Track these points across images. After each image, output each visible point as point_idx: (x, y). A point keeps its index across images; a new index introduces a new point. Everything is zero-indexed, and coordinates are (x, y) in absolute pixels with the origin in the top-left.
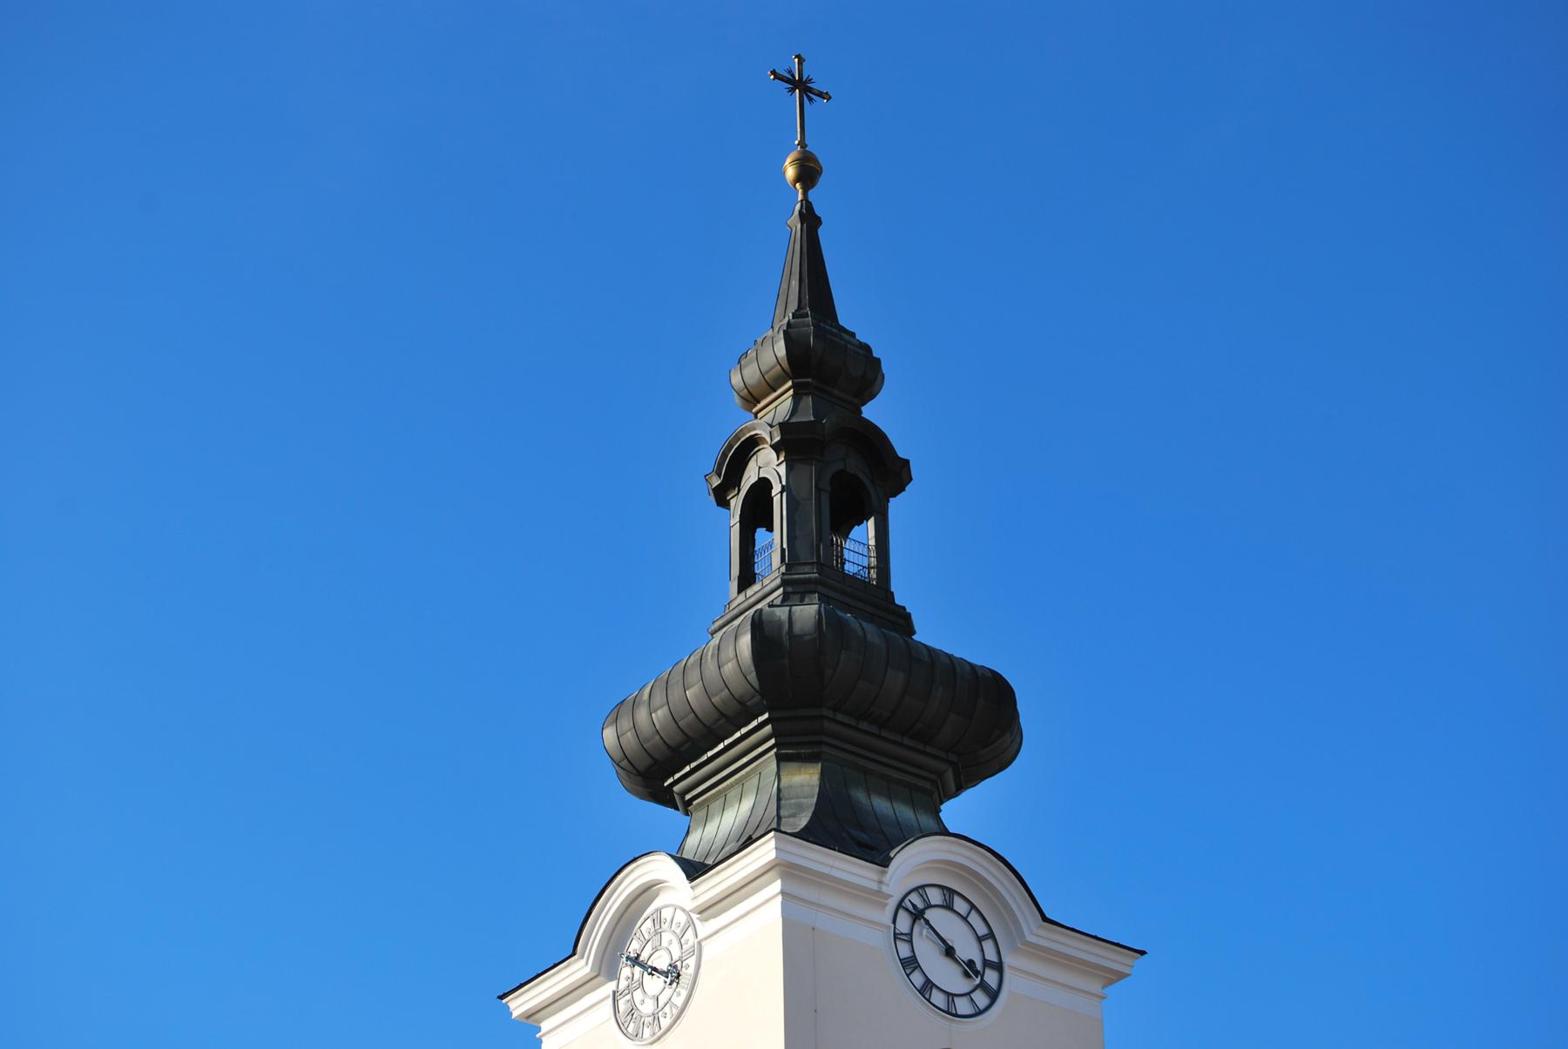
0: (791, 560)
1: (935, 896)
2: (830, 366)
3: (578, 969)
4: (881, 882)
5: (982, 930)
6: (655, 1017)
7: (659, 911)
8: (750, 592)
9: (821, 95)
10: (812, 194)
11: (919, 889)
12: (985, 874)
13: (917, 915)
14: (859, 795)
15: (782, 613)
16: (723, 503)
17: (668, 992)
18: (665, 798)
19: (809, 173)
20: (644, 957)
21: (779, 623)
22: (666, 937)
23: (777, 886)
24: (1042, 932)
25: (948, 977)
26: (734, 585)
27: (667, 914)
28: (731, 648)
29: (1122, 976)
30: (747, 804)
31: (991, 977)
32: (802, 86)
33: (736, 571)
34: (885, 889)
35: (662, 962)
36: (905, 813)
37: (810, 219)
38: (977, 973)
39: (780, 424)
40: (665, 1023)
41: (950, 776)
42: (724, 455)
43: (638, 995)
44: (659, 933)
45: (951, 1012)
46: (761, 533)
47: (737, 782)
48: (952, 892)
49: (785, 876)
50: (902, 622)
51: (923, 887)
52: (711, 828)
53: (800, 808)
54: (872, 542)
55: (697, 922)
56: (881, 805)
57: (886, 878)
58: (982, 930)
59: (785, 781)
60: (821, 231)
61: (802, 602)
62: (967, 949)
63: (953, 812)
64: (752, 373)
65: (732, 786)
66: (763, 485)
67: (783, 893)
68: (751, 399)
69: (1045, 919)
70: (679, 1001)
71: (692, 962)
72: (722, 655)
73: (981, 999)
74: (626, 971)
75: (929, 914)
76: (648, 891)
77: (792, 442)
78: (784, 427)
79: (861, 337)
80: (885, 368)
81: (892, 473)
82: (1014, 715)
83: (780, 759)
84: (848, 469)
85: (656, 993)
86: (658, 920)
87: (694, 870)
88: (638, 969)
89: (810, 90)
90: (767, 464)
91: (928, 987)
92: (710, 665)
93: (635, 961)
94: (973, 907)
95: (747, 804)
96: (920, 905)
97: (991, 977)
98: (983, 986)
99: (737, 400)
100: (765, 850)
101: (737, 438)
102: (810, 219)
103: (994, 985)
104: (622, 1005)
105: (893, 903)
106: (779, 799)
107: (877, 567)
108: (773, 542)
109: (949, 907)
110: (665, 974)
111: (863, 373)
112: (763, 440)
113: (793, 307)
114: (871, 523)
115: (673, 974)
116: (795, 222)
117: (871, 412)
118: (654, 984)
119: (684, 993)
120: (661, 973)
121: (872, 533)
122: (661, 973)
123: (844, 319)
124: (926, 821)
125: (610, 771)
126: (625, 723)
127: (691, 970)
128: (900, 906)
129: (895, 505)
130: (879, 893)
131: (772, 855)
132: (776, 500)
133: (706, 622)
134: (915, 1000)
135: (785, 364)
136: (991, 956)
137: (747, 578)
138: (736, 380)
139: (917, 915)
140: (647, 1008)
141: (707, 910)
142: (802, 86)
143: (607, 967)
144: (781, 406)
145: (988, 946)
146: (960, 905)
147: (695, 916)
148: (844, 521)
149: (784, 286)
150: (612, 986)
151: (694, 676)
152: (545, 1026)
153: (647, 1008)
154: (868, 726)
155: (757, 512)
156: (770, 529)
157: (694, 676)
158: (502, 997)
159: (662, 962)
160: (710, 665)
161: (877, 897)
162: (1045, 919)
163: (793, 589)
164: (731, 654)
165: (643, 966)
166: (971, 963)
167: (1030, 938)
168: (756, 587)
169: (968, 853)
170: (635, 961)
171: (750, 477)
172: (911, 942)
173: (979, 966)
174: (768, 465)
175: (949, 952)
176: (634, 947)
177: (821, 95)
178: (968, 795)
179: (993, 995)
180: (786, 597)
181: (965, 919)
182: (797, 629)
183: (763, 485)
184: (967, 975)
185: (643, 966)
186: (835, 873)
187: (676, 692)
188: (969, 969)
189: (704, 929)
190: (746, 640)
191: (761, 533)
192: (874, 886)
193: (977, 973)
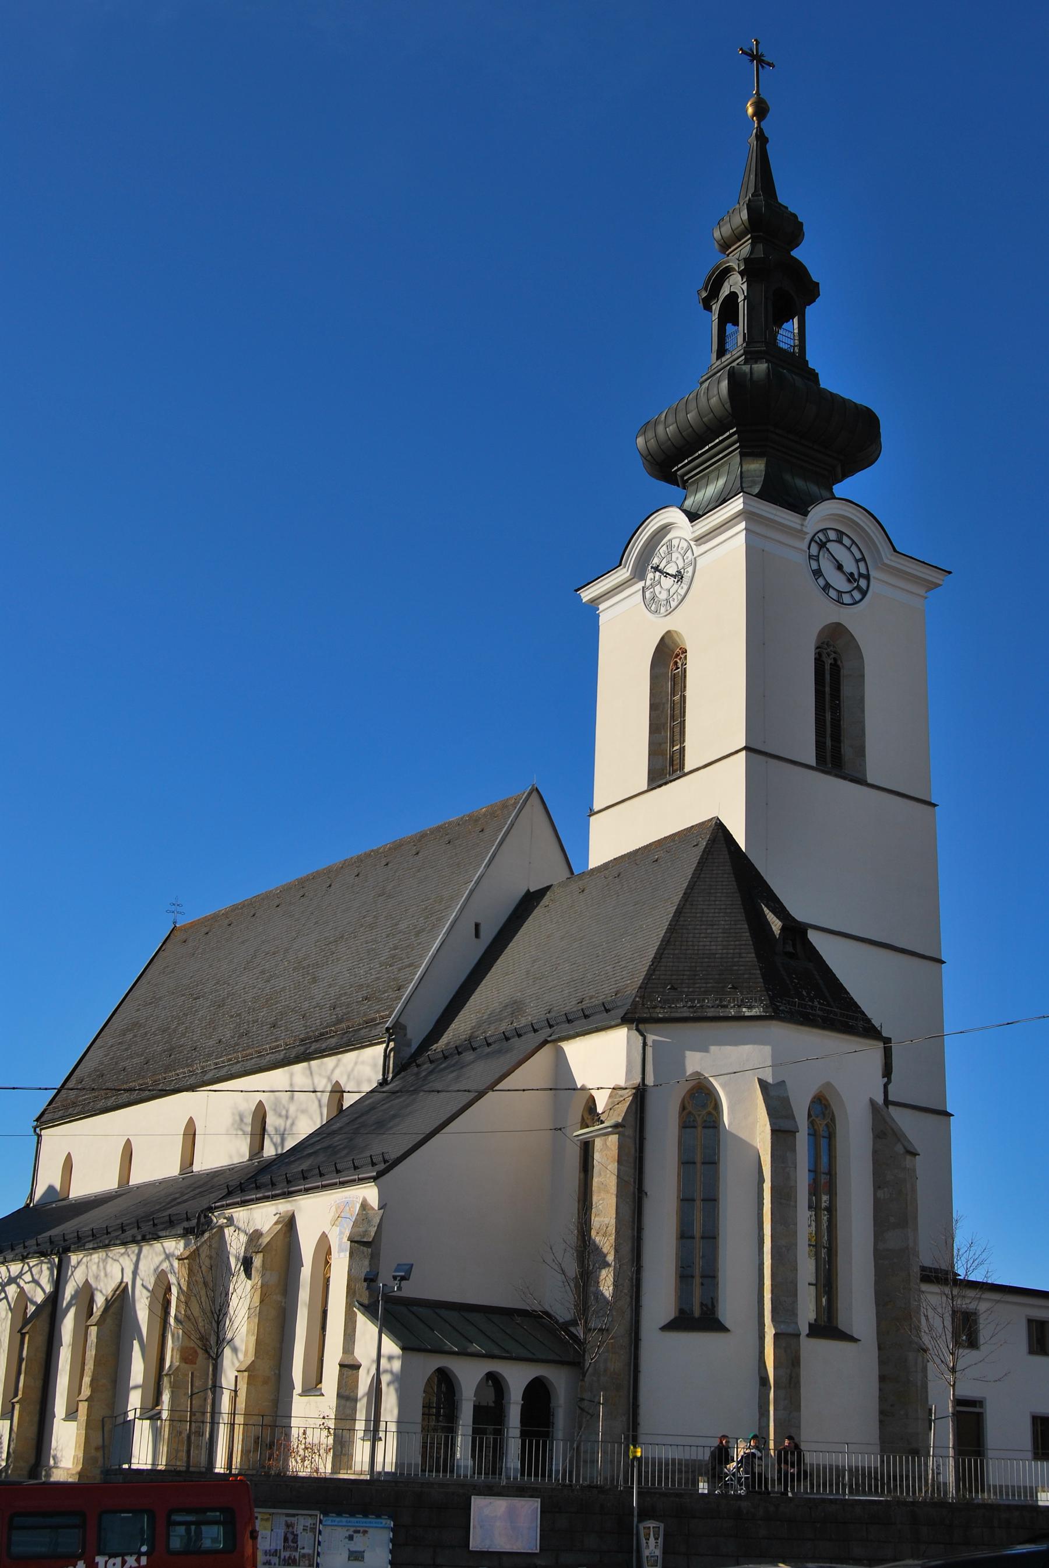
0: (749, 339)
1: (832, 535)
2: (772, 228)
3: (622, 574)
4: (802, 525)
5: (858, 556)
6: (668, 601)
7: (670, 540)
8: (723, 359)
9: (769, 64)
10: (763, 124)
11: (824, 531)
13: (822, 545)
14: (788, 477)
15: (746, 368)
16: (708, 307)
17: (676, 586)
18: (671, 479)
19: (761, 111)
20: (661, 567)
21: (744, 374)
22: (675, 556)
23: (743, 525)
24: (893, 558)
25: (839, 582)
26: (714, 355)
27: (675, 542)
28: (715, 389)
29: (937, 585)
30: (721, 482)
31: (863, 583)
32: (758, 58)
33: (715, 347)
34: (805, 529)
35: (672, 570)
36: (814, 489)
37: (762, 139)
38: (855, 580)
39: (745, 259)
40: (674, 604)
41: (839, 470)
42: (713, 273)
43: (657, 589)
44: (670, 553)
45: (839, 601)
46: (730, 328)
47: (716, 469)
49: (747, 520)
50: (813, 376)
52: (700, 496)
53: (754, 483)
54: (796, 331)
55: (694, 547)
56: (800, 483)
57: (806, 523)
58: (858, 556)
59: (745, 467)
61: (756, 363)
62: (850, 566)
63: (838, 489)
64: (726, 230)
65: (712, 471)
66: (733, 296)
67: (746, 529)
68: (726, 246)
69: (895, 550)
70: (682, 592)
71: (690, 569)
72: (710, 393)
73: (857, 595)
74: (650, 575)
75: (829, 545)
76: (665, 529)
77: (751, 270)
78: (746, 261)
81: (810, 291)
82: (878, 435)
83: (742, 455)
84: (782, 286)
85: (668, 587)
86: (670, 546)
87: (693, 516)
88: (658, 574)
89: (763, 61)
90: (736, 283)
91: (827, 587)
92: (703, 399)
93: (656, 569)
94: (853, 542)
95: (721, 482)
96: (824, 540)
97: (863, 583)
98: (858, 588)
99: (716, 246)
100: (737, 504)
101: (717, 268)
102: (762, 139)
103: (865, 588)
104: (648, 595)
105: (808, 537)
106: (741, 478)
107: (799, 345)
108: (738, 334)
109: (840, 541)
110: (674, 576)
112: (733, 269)
113: (752, 190)
114: (796, 320)
115: (679, 576)
116: (753, 140)
118: (667, 582)
119: (685, 587)
120: (672, 576)
121: (796, 326)
122: (672, 576)
124: (827, 494)
125: (639, 462)
126: (650, 434)
127: (690, 574)
128: (812, 540)
129: (809, 310)
130: (801, 531)
131: (741, 506)
132: (741, 304)
133: (699, 378)
135: (747, 224)
136: (863, 571)
137: (721, 352)
138: (717, 234)
139: (822, 545)
140: (663, 596)
141: (700, 540)
142: (758, 58)
143: (639, 573)
144: (744, 249)
145: (862, 565)
146: (846, 541)
147: (692, 543)
148: (782, 317)
149: (746, 179)
150: (641, 584)
151: (692, 405)
152: (601, 607)
153: (663, 596)
154: (792, 441)
155: (729, 313)
156: (736, 324)
157: (692, 405)
158: (577, 590)
159: (672, 570)
160: (703, 399)
161: (800, 533)
162: (895, 550)
163: (751, 356)
164: (716, 392)
165: (661, 571)
166: (852, 574)
167: (886, 561)
168: (728, 356)
169: (851, 510)
170: (656, 569)
171: (725, 291)
172: (818, 560)
173: (856, 576)
174: (736, 284)
175: (840, 567)
176: (655, 561)
177: (769, 64)
178: (848, 481)
179: (864, 593)
180: (746, 362)
181: (849, 549)
182: (755, 376)
183: (733, 296)
184: (849, 581)
185: (661, 571)
186: (776, 518)
187: (681, 415)
188: (851, 578)
189: (698, 550)
190: (724, 384)
191: (730, 328)
192: (799, 527)
193: (855, 580)
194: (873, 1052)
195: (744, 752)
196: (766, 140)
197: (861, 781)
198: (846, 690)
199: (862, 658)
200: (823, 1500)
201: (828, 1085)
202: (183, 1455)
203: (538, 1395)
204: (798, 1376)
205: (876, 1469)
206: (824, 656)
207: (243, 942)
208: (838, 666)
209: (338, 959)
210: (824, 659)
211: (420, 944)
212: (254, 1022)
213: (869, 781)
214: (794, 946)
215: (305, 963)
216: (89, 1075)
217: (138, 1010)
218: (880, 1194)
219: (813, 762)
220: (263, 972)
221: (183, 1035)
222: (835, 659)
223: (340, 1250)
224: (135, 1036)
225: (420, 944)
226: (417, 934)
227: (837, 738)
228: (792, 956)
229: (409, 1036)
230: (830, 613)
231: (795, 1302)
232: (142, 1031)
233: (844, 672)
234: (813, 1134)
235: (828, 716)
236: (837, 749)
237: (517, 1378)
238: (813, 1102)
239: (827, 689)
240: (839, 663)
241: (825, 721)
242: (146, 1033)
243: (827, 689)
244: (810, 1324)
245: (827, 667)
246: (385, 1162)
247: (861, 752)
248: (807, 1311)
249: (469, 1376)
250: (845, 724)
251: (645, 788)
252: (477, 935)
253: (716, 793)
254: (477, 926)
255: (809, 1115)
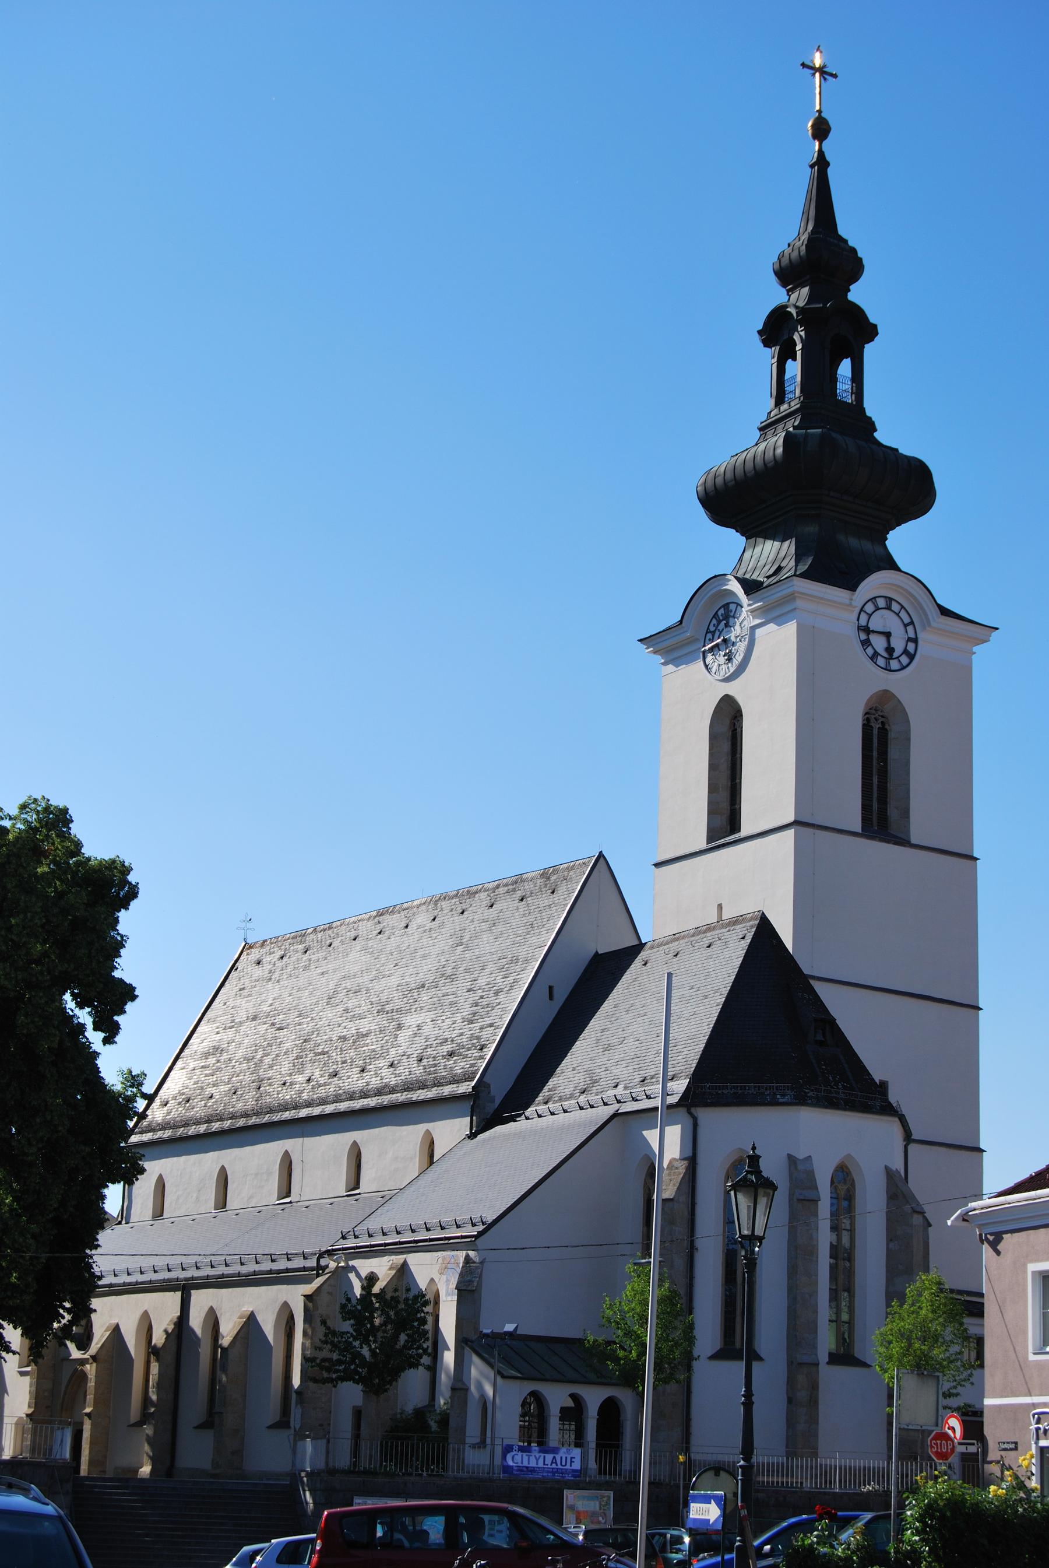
1: (881, 603)
5: (907, 620)
9: (832, 75)
12: (911, 591)
14: (841, 538)
19: (821, 130)
46: (789, 362)
48: (891, 599)
50: (870, 426)
51: (875, 598)
56: (854, 542)
57: (854, 597)
58: (907, 620)
60: (830, 171)
79: (851, 243)
80: (865, 262)
89: (826, 73)
94: (902, 607)
102: (821, 163)
105: (857, 610)
109: (888, 608)
111: (852, 266)
117: (857, 294)
123: (842, 231)
128: (862, 610)
134: (869, 664)
146: (895, 607)
156: (795, 359)
166: (893, 650)
177: (832, 75)
181: (898, 614)
186: (738, 1319)
191: (789, 362)
194: (891, 1127)
195: (790, 833)
196: (828, 164)
197: (904, 841)
198: (893, 753)
199: (908, 721)
200: (825, 1493)
201: (849, 1156)
202: (323, 1458)
203: (610, 1410)
204: (817, 1395)
205: (883, 1468)
206: (872, 720)
207: (323, 973)
208: (886, 730)
209: (422, 1008)
210: (872, 724)
211: (499, 1004)
212: (344, 1062)
213: (913, 841)
214: (824, 1035)
215: (388, 1008)
216: (174, 1098)
217: (218, 1033)
218: (891, 1245)
219: (858, 828)
220: (346, 1010)
221: (271, 1067)
222: (883, 723)
223: (448, 1294)
224: (218, 1061)
225: (499, 1004)
226: (497, 993)
227: (883, 800)
228: (821, 1043)
229: (492, 1093)
230: (876, 679)
231: (816, 1338)
232: (225, 1057)
233: (891, 735)
234: (835, 1197)
235: (875, 780)
236: (882, 813)
237: (594, 1397)
238: (836, 1171)
239: (875, 754)
240: (887, 727)
241: (871, 785)
242: (230, 1059)
243: (875, 754)
244: (830, 1354)
245: (875, 732)
246: (483, 1223)
247: (906, 813)
248: (826, 1341)
249: (557, 1396)
250: (891, 786)
251: (703, 844)
252: (551, 997)
253: (762, 881)
254: (551, 988)
255: (832, 1182)
